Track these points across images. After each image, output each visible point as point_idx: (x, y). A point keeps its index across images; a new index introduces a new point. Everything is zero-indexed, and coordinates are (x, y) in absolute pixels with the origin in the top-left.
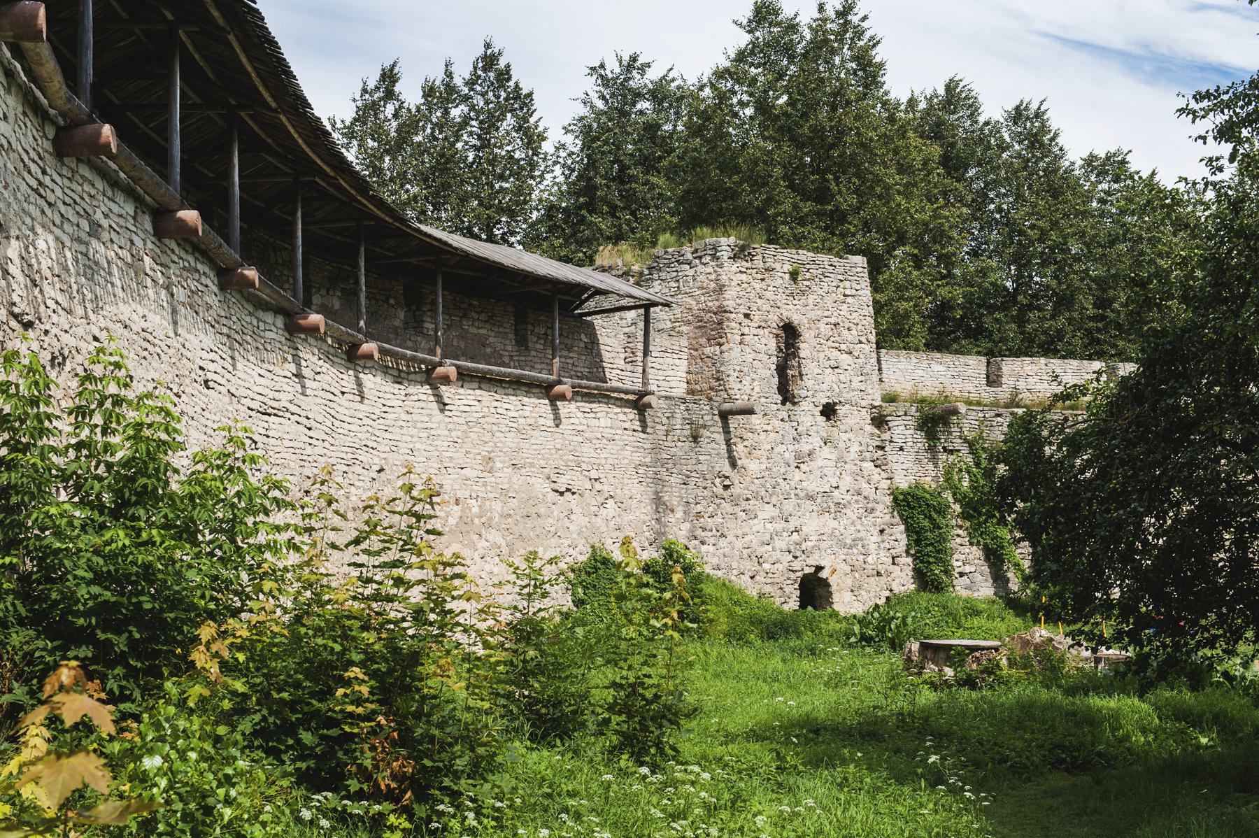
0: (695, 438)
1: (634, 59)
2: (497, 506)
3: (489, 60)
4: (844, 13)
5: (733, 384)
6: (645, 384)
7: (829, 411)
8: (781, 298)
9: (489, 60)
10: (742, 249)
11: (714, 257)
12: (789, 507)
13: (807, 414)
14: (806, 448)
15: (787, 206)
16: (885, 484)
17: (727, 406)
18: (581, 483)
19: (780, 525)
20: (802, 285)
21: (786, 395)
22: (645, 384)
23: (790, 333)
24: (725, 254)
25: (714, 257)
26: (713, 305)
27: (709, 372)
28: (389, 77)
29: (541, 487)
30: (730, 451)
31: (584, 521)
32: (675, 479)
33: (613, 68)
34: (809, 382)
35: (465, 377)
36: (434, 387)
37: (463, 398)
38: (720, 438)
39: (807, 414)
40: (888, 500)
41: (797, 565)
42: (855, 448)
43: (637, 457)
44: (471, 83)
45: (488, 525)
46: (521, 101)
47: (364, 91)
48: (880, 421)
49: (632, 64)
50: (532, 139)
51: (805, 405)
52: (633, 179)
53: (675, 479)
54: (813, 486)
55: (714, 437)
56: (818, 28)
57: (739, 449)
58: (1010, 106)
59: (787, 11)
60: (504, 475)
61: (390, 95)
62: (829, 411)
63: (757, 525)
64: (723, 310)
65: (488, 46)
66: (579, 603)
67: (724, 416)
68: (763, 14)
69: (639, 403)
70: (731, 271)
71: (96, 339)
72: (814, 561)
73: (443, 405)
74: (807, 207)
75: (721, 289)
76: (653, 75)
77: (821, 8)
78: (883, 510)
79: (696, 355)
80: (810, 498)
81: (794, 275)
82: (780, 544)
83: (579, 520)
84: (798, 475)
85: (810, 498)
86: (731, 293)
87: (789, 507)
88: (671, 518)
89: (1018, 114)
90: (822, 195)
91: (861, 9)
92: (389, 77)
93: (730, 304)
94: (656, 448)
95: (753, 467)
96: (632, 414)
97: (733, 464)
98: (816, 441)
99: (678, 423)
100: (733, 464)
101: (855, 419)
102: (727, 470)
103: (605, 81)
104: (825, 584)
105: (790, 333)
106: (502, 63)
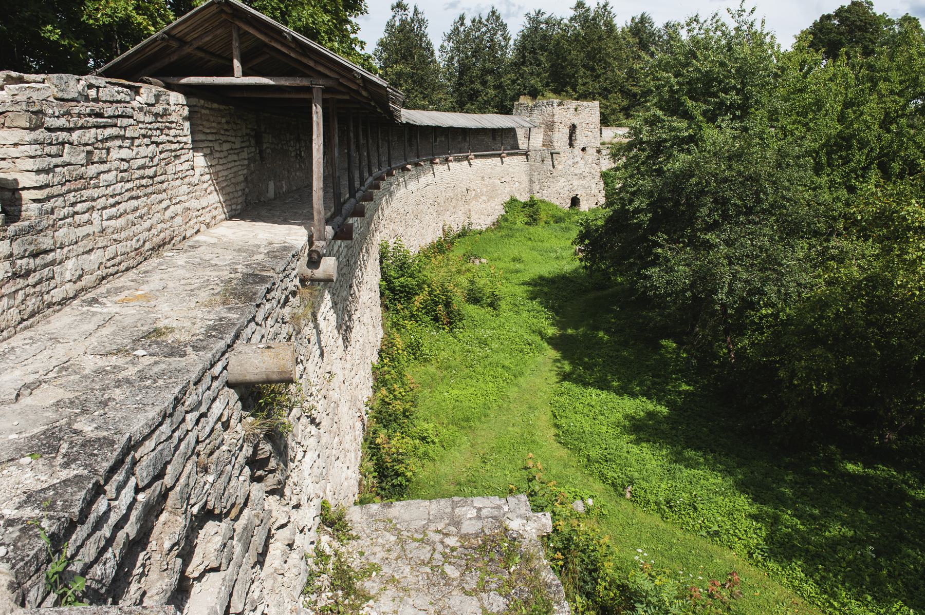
0: (543, 161)
1: (540, 11)
2: (485, 190)
3: (493, 13)
4: (605, 6)
5: (555, 144)
6: (528, 148)
7: (583, 149)
8: (571, 117)
9: (493, 13)
10: (561, 103)
11: (552, 106)
12: (569, 178)
13: (577, 151)
14: (576, 161)
15: (582, 73)
16: (599, 170)
17: (553, 151)
18: (507, 179)
19: (566, 184)
20: (578, 112)
21: (571, 145)
22: (528, 148)
23: (573, 128)
24: (555, 105)
25: (552, 106)
26: (551, 120)
27: (549, 139)
28: (462, 18)
29: (497, 182)
30: (553, 163)
31: (509, 189)
32: (536, 174)
33: (533, 14)
34: (578, 141)
35: (476, 157)
36: (468, 161)
37: (477, 163)
38: (550, 160)
39: (577, 151)
40: (599, 174)
41: (570, 194)
42: (590, 160)
43: (525, 169)
44: (487, 20)
45: (482, 195)
46: (504, 27)
47: (454, 23)
48: (599, 151)
49: (539, 13)
50: (506, 39)
51: (576, 148)
52: (537, 53)
53: (536, 174)
54: (577, 172)
55: (548, 162)
56: (596, 12)
57: (556, 163)
58: (665, 22)
59: (587, 5)
60: (487, 181)
61: (462, 24)
62: (583, 149)
63: (560, 184)
64: (553, 122)
65: (493, 8)
66: (506, 212)
67: (552, 154)
68: (580, 5)
69: (526, 154)
70: (557, 109)
71: (454, 352)
72: (576, 193)
73: (470, 165)
74: (588, 73)
75: (553, 115)
76: (546, 16)
77: (598, 4)
78: (597, 178)
79: (546, 135)
80: (576, 175)
81: (576, 110)
82: (566, 189)
83: (508, 189)
84: (573, 169)
85: (576, 175)
86: (556, 117)
87: (569, 178)
88: (534, 185)
89: (667, 25)
90: (593, 69)
91: (610, 5)
92: (462, 18)
93: (555, 120)
94: (531, 166)
95: (559, 167)
96: (524, 157)
97: (554, 167)
98: (579, 159)
99: (538, 157)
100: (554, 167)
101: (591, 151)
102: (552, 169)
103: (530, 18)
104: (579, 199)
105: (573, 128)
106: (497, 14)
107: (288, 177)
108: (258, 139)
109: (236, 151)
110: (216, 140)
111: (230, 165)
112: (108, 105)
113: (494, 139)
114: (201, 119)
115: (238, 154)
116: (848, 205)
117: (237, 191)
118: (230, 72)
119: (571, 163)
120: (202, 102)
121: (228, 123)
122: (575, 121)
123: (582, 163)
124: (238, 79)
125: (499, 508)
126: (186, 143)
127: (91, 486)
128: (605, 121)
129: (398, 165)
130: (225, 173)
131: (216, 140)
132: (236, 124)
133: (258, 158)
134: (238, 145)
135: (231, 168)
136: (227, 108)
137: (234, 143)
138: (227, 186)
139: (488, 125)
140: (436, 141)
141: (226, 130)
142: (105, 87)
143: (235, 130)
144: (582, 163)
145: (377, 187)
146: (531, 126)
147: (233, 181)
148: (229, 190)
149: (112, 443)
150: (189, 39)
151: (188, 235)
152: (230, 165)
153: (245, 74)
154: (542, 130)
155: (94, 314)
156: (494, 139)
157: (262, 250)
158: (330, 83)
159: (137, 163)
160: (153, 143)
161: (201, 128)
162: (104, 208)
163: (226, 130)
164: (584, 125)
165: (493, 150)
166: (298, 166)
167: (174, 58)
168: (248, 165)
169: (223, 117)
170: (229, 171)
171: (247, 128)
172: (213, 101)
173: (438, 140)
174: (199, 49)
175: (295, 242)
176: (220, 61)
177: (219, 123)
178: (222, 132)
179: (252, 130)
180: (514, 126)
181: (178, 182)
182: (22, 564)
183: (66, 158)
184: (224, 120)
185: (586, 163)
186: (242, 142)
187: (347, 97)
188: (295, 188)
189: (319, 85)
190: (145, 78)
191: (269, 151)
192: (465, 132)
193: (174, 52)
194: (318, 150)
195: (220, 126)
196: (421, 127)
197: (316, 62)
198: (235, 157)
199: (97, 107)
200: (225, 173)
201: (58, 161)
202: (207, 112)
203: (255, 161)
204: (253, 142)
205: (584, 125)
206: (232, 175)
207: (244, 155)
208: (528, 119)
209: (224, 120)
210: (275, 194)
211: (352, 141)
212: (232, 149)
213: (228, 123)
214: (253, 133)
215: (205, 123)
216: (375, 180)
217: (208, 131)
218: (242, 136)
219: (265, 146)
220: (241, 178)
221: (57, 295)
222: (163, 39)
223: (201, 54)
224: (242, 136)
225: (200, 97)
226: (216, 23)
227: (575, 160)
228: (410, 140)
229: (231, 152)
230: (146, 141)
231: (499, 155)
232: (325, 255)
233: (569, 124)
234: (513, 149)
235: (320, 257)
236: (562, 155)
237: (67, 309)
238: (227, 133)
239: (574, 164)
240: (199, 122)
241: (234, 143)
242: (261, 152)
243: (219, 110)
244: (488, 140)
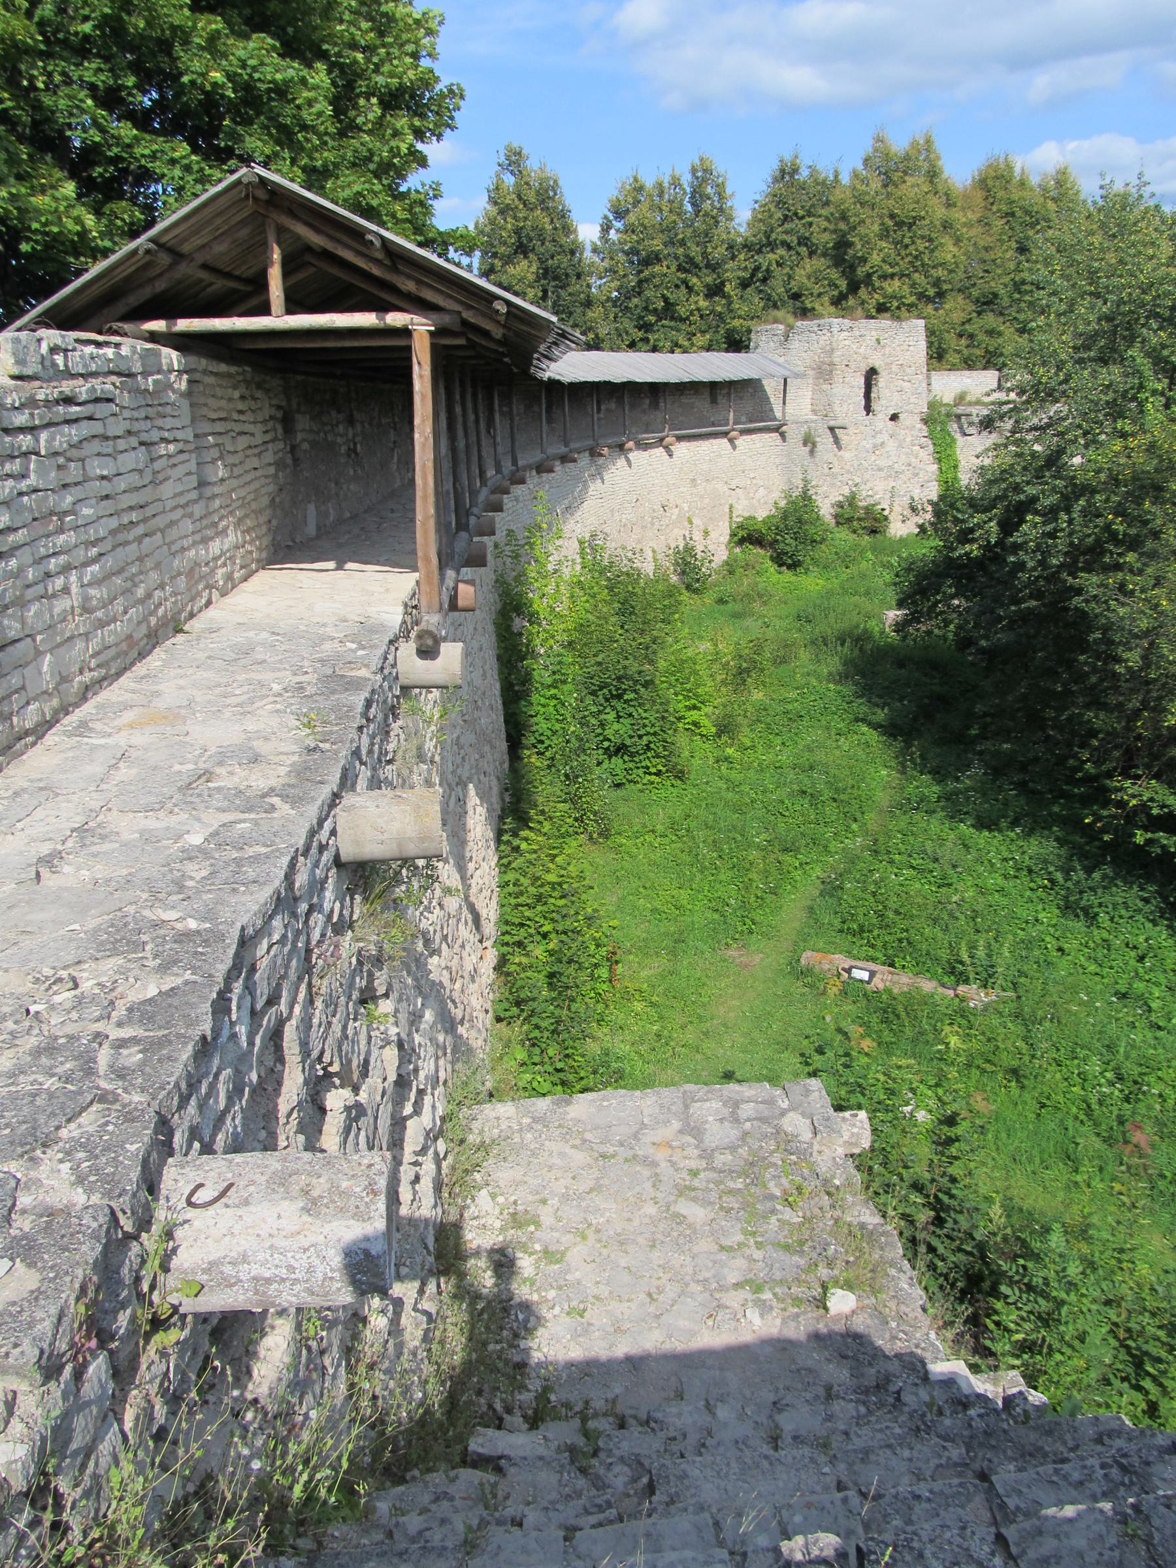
21: (868, 409)
31: (746, 502)
35: (680, 438)
37: (683, 450)
42: (909, 439)
43: (778, 461)
51: (880, 416)
54: (882, 463)
64: (832, 364)
67: (832, 429)
80: (880, 470)
85: (880, 470)
93: (836, 360)
96: (775, 435)
98: (884, 437)
107: (337, 495)
108: (287, 422)
109: (256, 451)
110: (227, 432)
111: (248, 477)
112: (81, 381)
113: (714, 401)
114: (204, 394)
115: (259, 455)
116: (80, 1126)
117: (259, 526)
118: (264, 309)
119: (869, 446)
120: (204, 362)
121: (243, 398)
122: (877, 361)
123: (891, 445)
124: (279, 320)
125: (771, 1102)
126: (186, 442)
127: (215, 995)
128: (937, 356)
129: (531, 461)
130: (242, 492)
131: (227, 432)
132: (255, 399)
133: (289, 461)
134: (259, 439)
135: (249, 483)
136: (240, 370)
137: (252, 435)
138: (246, 516)
139: (704, 376)
140: (599, 410)
141: (241, 412)
142: (74, 350)
143: (253, 411)
144: (891, 445)
145: (498, 508)
146: (787, 373)
147: (254, 506)
148: (249, 523)
149: (221, 937)
150: (186, 248)
151: (195, 610)
152: (248, 477)
153: (294, 305)
154: (810, 381)
155: (93, 749)
156: (714, 401)
157: (330, 631)
158: (446, 319)
159: (122, 484)
160: (142, 444)
161: (205, 411)
162: (86, 564)
163: (241, 412)
164: (894, 368)
165: (713, 425)
166: (351, 472)
167: (160, 286)
168: (275, 476)
169: (235, 387)
170: (248, 489)
171: (271, 406)
172: (219, 358)
173: (603, 407)
174: (205, 266)
175: (385, 616)
176: (232, 284)
177: (230, 400)
178: (235, 416)
179: (279, 407)
180: (754, 375)
181: (179, 513)
182: (164, 1093)
183: (32, 480)
184: (236, 394)
185: (901, 446)
186: (266, 432)
187: (461, 341)
188: (348, 515)
189: (421, 326)
190: (116, 325)
191: (305, 446)
192: (655, 391)
193: (161, 275)
194: (424, 445)
195: (231, 406)
196: (571, 384)
197: (419, 282)
198: (255, 462)
199: (67, 387)
200: (242, 492)
201: (24, 485)
202: (210, 380)
203: (285, 466)
204: (280, 431)
205: (894, 368)
206: (252, 496)
207: (269, 457)
208: (781, 360)
209: (236, 394)
210: (319, 528)
211: (460, 419)
212: (250, 447)
213: (243, 398)
214: (279, 415)
215: (210, 401)
216: (493, 492)
217: (214, 416)
218: (264, 422)
219: (300, 436)
220: (265, 501)
221: (31, 716)
222: (148, 252)
223: (204, 275)
224: (264, 422)
225: (200, 353)
226: (238, 218)
227: (879, 441)
228: (549, 410)
229: (249, 452)
230: (134, 442)
231: (725, 434)
232: (445, 639)
233: (864, 368)
234: (751, 421)
235: (437, 641)
236: (851, 431)
237: (51, 738)
238: (242, 418)
239: (875, 447)
240: (202, 400)
241: (252, 435)
242: (293, 449)
243: (229, 375)
244: (701, 404)
